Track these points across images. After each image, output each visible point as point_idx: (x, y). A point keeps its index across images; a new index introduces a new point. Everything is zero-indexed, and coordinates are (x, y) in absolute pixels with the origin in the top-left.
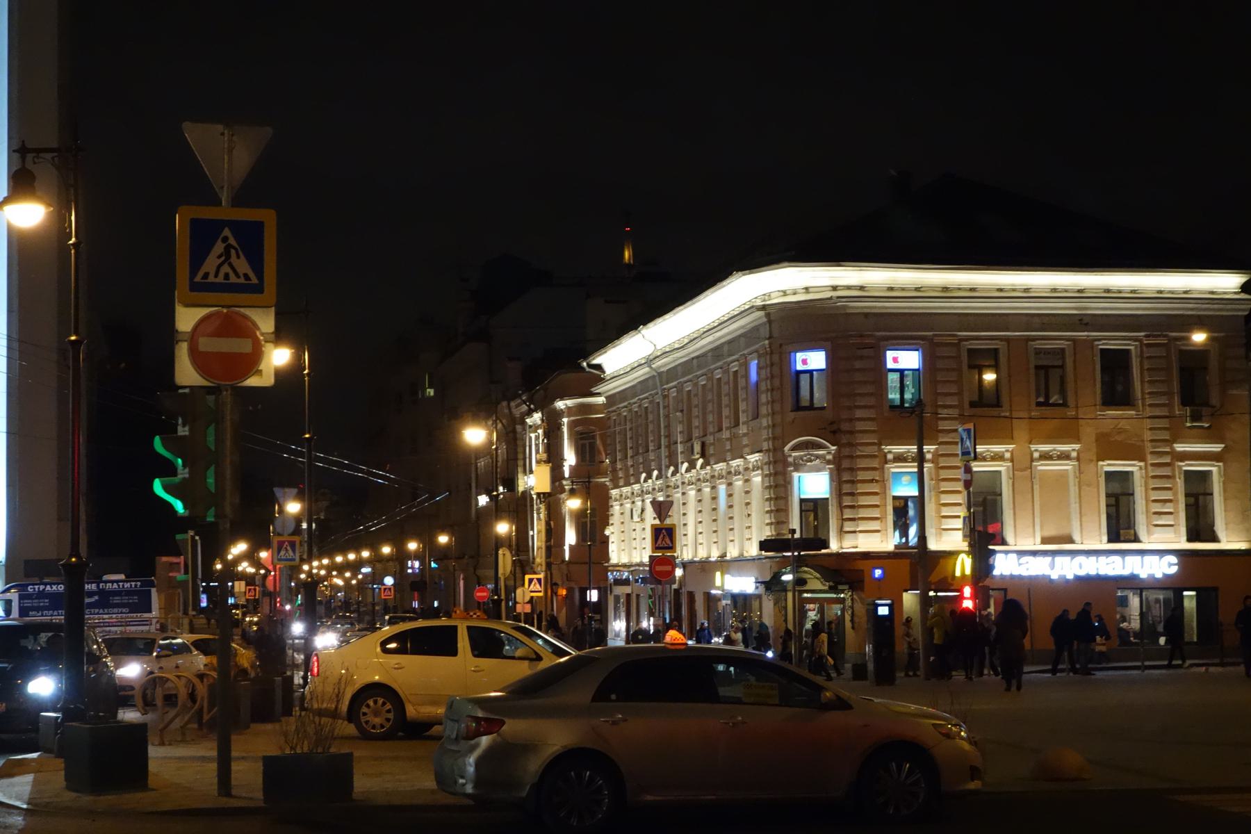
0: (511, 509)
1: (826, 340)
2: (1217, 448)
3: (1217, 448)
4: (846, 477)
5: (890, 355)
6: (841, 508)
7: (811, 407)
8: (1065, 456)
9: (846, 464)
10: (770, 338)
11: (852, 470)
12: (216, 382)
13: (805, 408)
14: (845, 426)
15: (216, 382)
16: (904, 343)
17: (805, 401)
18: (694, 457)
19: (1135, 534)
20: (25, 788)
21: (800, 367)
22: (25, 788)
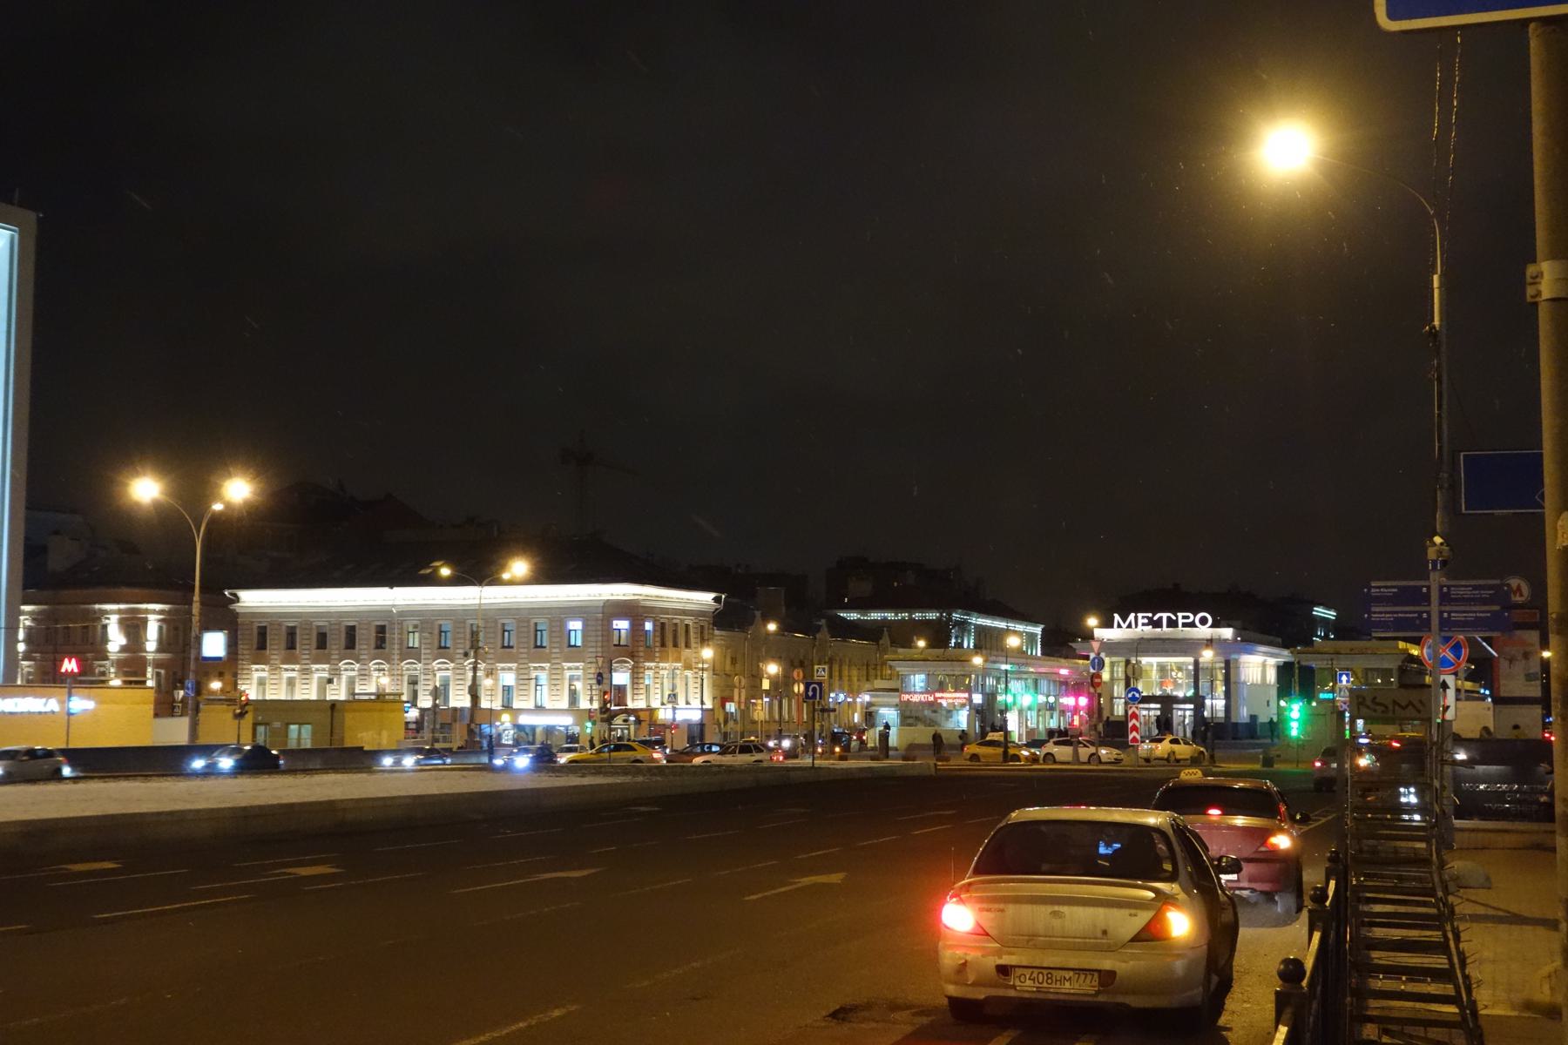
0: (796, 697)
1: (631, 616)
2: (971, 647)
3: (971, 647)
4: (636, 676)
5: (615, 622)
6: (633, 689)
7: (619, 645)
8: (577, 668)
9: (635, 670)
10: (603, 613)
11: (637, 673)
12: (1395, 583)
13: (572, 646)
14: (636, 654)
15: (1395, 583)
16: (574, 618)
17: (572, 643)
18: (1426, 647)
19: (1358, 699)
20: (1195, 991)
21: (615, 627)
22: (1195, 991)
